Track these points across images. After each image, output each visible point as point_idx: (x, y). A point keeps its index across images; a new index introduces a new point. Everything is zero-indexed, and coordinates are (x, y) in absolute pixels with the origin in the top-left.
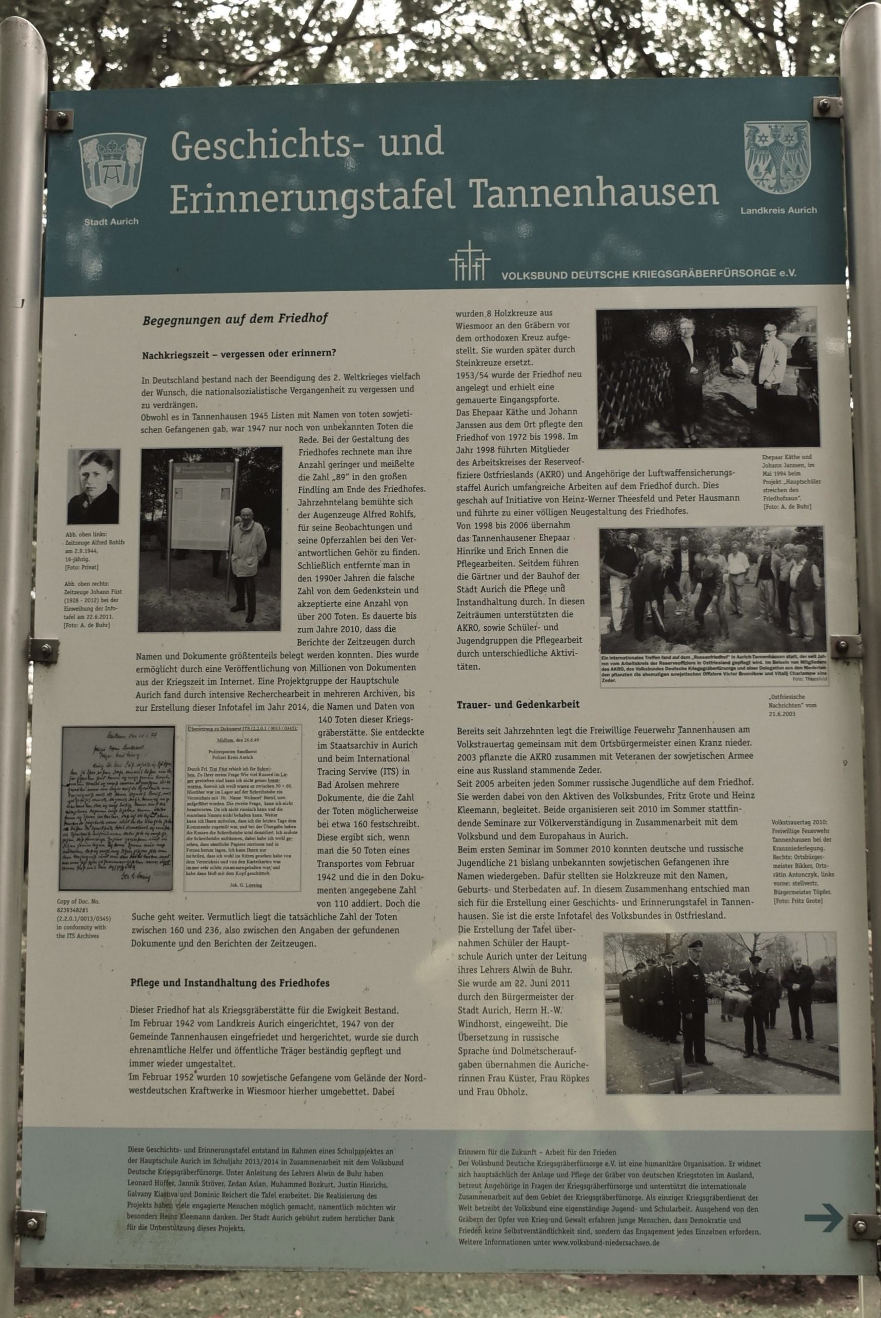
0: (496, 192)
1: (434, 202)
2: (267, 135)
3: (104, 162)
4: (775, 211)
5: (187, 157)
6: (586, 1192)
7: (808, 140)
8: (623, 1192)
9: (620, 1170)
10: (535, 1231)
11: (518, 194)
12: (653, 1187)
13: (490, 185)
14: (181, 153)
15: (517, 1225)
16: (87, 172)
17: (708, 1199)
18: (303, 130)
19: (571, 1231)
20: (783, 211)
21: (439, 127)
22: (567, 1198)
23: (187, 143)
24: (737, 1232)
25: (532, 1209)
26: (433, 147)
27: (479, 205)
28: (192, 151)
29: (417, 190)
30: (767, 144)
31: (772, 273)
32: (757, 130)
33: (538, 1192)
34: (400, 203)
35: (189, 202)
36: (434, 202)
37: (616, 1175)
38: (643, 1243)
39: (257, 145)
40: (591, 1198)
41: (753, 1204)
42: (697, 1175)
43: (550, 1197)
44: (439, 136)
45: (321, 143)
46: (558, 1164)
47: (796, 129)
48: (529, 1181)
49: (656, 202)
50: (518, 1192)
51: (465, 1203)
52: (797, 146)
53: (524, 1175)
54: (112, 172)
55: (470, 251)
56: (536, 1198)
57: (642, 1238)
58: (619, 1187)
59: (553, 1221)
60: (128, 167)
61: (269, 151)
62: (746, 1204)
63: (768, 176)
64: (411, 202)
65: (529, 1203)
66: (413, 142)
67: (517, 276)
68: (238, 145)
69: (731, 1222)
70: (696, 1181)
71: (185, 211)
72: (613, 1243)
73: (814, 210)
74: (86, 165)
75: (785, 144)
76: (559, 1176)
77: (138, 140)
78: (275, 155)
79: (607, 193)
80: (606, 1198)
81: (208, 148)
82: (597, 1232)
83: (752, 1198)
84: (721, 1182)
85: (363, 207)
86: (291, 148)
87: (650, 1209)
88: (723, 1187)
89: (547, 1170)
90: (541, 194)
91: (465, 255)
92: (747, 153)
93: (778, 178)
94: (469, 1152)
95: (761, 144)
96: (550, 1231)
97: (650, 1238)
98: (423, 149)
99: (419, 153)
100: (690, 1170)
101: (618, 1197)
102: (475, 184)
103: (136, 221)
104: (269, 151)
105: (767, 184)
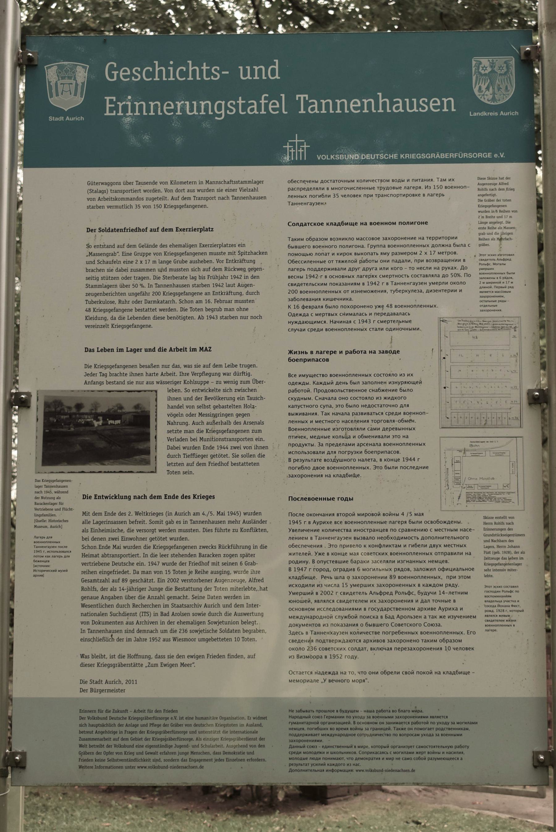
0: (314, 103)
1: (274, 110)
2: (167, 66)
3: (61, 81)
4: (491, 114)
5: (115, 79)
6: (158, 736)
7: (513, 70)
8: (182, 736)
9: (180, 722)
10: (126, 760)
11: (327, 104)
12: (200, 733)
13: (309, 99)
14: (111, 76)
15: (115, 757)
16: (50, 87)
17: (234, 740)
18: (190, 62)
19: (149, 760)
20: (497, 114)
21: (277, 61)
22: (147, 739)
23: (115, 70)
24: (252, 760)
25: (125, 746)
26: (273, 74)
27: (302, 111)
28: (118, 75)
29: (263, 102)
30: (487, 72)
31: (489, 155)
32: (481, 63)
33: (129, 736)
34: (252, 110)
35: (116, 108)
36: (274, 110)
37: (177, 725)
38: (193, 767)
39: (160, 72)
40: (162, 740)
41: (262, 743)
42: (227, 725)
43: (136, 739)
44: (277, 67)
45: (201, 71)
46: (142, 719)
47: (505, 62)
48: (122, 729)
49: (415, 110)
50: (116, 736)
51: (83, 743)
52: (505, 74)
53: (120, 725)
54: (66, 88)
55: (297, 141)
56: (127, 739)
57: (193, 764)
58: (178, 732)
59: (137, 754)
60: (77, 85)
61: (168, 76)
62: (257, 743)
63: (487, 93)
64: (259, 109)
65: (122, 743)
66: (260, 71)
67: (327, 157)
68: (148, 71)
69: (248, 753)
70: (227, 729)
71: (114, 114)
72: (174, 767)
73: (516, 113)
74: (49, 82)
75: (499, 72)
76: (142, 726)
77: (83, 67)
78: (172, 79)
79: (384, 104)
80: (171, 739)
81: (129, 73)
82: (165, 760)
83: (261, 739)
84: (242, 729)
85: (228, 112)
86: (182, 74)
87: (198, 746)
88: (243, 732)
89: (134, 722)
90: (342, 104)
91: (293, 144)
92: (474, 78)
93: (494, 94)
94: (85, 711)
95: (483, 72)
96: (135, 760)
97: (198, 764)
98: (266, 75)
99: (264, 78)
100: (222, 722)
101: (178, 739)
102: (300, 98)
103: (82, 118)
104: (168, 76)
105: (486, 97)
